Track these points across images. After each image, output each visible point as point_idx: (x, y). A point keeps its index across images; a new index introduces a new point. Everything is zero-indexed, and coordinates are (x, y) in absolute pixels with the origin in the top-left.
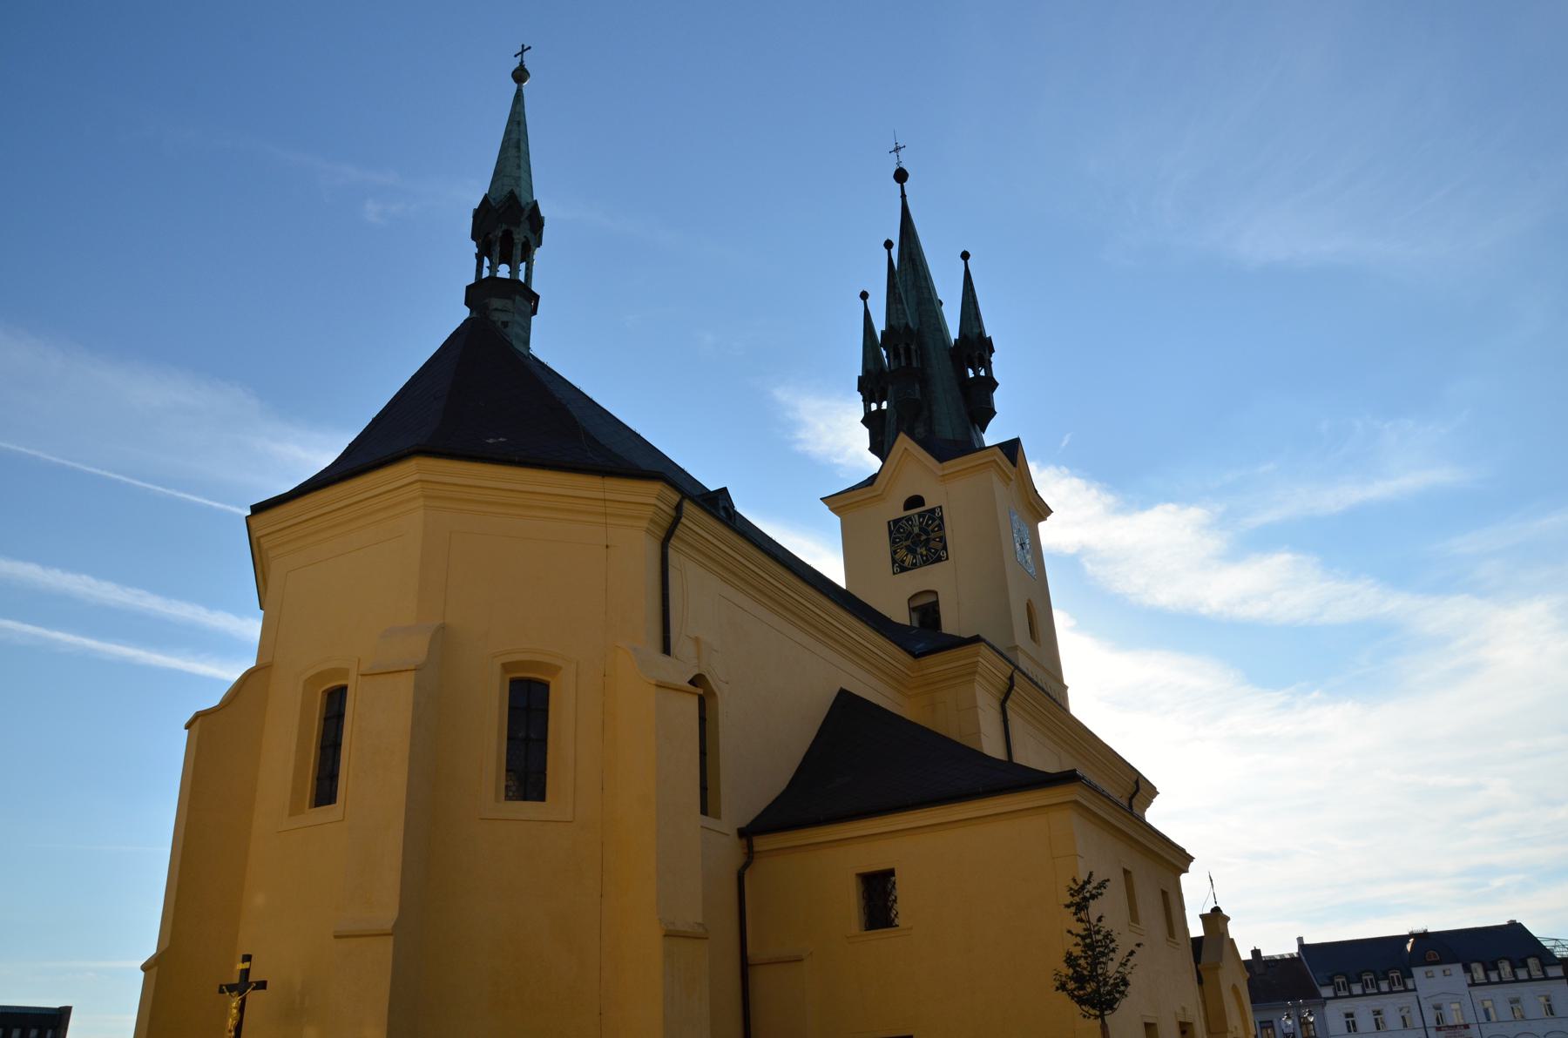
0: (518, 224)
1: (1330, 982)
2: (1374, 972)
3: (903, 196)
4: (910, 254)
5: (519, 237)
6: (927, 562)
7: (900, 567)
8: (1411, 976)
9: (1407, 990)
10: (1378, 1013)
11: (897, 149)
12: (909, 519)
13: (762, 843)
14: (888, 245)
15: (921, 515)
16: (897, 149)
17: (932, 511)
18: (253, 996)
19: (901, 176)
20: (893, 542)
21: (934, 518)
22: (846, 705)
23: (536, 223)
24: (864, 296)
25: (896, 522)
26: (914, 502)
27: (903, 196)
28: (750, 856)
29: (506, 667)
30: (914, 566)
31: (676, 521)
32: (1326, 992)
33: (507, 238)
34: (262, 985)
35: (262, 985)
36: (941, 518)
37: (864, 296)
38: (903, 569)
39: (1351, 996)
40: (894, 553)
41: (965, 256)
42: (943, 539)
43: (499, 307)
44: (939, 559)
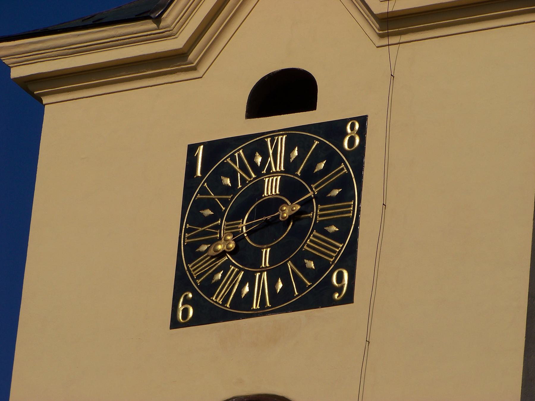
6: (282, 303)
12: (256, 144)
17: (335, 130)
21: (332, 162)
25: (216, 149)
36: (357, 157)
40: (189, 252)
44: (322, 296)
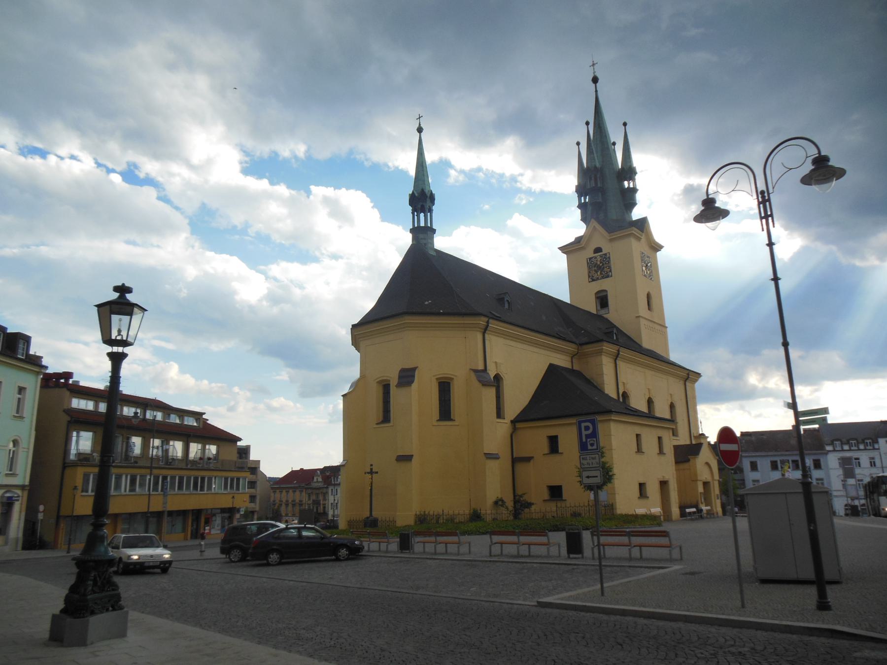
0: (426, 202)
1: (832, 443)
2: (841, 441)
3: (596, 91)
4: (599, 124)
5: (427, 207)
6: (603, 278)
7: (593, 279)
8: (877, 442)
9: (874, 449)
10: (873, 458)
11: (593, 65)
13: (518, 425)
14: (587, 123)
15: (601, 256)
16: (593, 65)
17: (605, 254)
18: (374, 475)
19: (595, 80)
20: (589, 268)
21: (606, 259)
22: (552, 369)
23: (432, 198)
24: (578, 144)
25: (590, 259)
26: (598, 250)
27: (596, 91)
28: (514, 430)
29: (437, 379)
30: (598, 279)
31: (487, 326)
32: (829, 448)
33: (423, 207)
34: (377, 473)
35: (377, 473)
37: (578, 144)
38: (593, 280)
39: (859, 450)
41: (625, 124)
42: (610, 267)
43: (422, 234)
44: (608, 277)
